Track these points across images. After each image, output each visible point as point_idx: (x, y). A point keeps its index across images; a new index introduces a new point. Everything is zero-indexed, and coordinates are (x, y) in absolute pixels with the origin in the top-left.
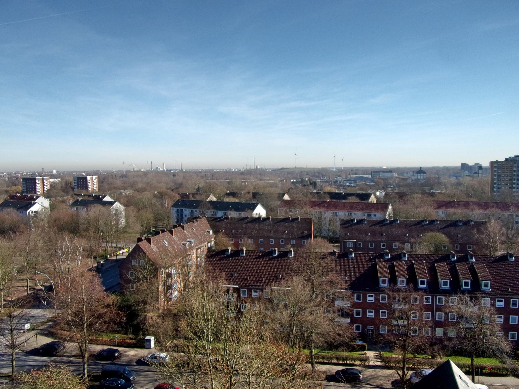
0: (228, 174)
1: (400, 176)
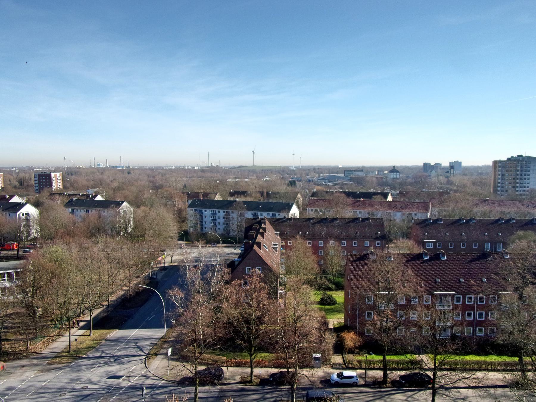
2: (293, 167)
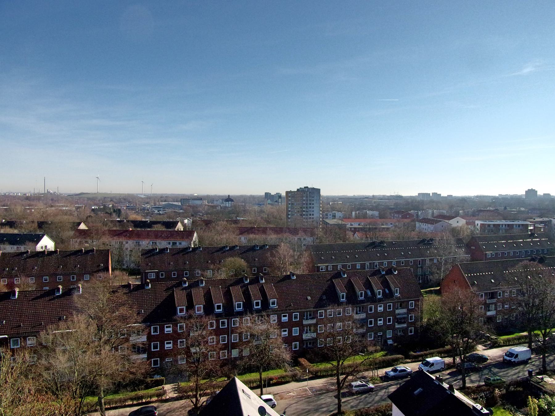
1: (210, 204)
2: (142, 194)
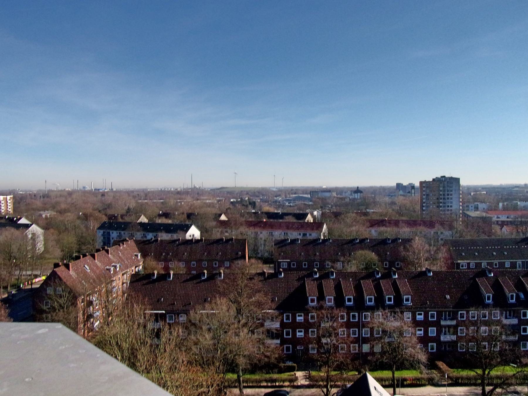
0: (163, 194)
